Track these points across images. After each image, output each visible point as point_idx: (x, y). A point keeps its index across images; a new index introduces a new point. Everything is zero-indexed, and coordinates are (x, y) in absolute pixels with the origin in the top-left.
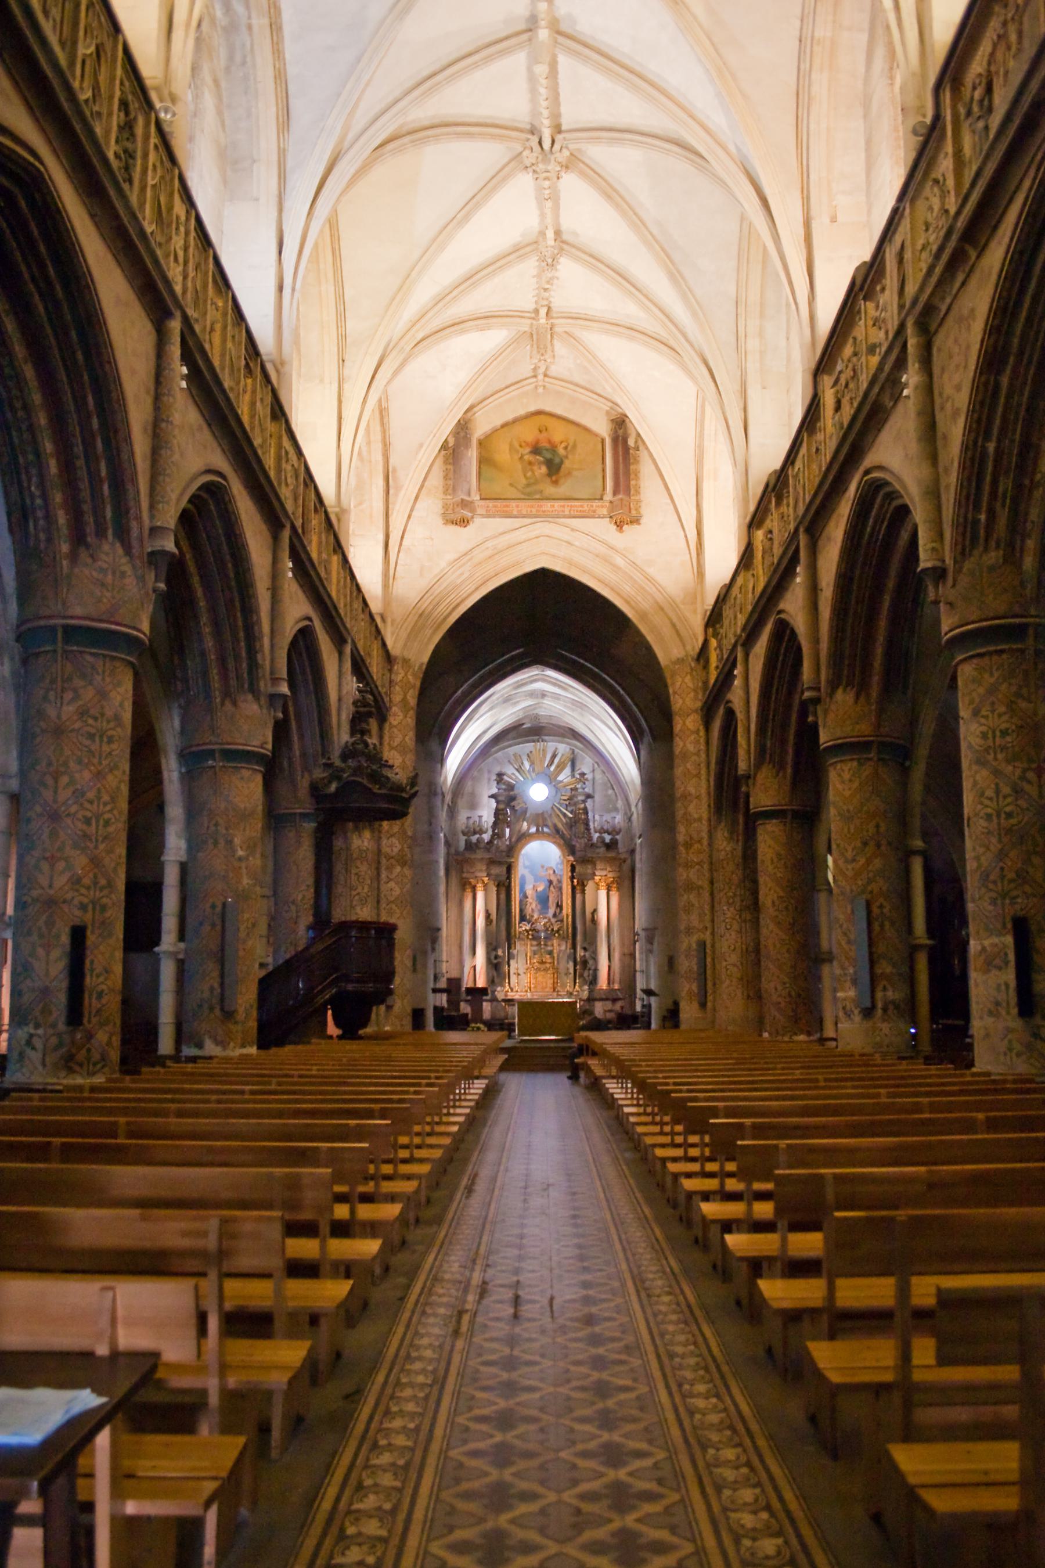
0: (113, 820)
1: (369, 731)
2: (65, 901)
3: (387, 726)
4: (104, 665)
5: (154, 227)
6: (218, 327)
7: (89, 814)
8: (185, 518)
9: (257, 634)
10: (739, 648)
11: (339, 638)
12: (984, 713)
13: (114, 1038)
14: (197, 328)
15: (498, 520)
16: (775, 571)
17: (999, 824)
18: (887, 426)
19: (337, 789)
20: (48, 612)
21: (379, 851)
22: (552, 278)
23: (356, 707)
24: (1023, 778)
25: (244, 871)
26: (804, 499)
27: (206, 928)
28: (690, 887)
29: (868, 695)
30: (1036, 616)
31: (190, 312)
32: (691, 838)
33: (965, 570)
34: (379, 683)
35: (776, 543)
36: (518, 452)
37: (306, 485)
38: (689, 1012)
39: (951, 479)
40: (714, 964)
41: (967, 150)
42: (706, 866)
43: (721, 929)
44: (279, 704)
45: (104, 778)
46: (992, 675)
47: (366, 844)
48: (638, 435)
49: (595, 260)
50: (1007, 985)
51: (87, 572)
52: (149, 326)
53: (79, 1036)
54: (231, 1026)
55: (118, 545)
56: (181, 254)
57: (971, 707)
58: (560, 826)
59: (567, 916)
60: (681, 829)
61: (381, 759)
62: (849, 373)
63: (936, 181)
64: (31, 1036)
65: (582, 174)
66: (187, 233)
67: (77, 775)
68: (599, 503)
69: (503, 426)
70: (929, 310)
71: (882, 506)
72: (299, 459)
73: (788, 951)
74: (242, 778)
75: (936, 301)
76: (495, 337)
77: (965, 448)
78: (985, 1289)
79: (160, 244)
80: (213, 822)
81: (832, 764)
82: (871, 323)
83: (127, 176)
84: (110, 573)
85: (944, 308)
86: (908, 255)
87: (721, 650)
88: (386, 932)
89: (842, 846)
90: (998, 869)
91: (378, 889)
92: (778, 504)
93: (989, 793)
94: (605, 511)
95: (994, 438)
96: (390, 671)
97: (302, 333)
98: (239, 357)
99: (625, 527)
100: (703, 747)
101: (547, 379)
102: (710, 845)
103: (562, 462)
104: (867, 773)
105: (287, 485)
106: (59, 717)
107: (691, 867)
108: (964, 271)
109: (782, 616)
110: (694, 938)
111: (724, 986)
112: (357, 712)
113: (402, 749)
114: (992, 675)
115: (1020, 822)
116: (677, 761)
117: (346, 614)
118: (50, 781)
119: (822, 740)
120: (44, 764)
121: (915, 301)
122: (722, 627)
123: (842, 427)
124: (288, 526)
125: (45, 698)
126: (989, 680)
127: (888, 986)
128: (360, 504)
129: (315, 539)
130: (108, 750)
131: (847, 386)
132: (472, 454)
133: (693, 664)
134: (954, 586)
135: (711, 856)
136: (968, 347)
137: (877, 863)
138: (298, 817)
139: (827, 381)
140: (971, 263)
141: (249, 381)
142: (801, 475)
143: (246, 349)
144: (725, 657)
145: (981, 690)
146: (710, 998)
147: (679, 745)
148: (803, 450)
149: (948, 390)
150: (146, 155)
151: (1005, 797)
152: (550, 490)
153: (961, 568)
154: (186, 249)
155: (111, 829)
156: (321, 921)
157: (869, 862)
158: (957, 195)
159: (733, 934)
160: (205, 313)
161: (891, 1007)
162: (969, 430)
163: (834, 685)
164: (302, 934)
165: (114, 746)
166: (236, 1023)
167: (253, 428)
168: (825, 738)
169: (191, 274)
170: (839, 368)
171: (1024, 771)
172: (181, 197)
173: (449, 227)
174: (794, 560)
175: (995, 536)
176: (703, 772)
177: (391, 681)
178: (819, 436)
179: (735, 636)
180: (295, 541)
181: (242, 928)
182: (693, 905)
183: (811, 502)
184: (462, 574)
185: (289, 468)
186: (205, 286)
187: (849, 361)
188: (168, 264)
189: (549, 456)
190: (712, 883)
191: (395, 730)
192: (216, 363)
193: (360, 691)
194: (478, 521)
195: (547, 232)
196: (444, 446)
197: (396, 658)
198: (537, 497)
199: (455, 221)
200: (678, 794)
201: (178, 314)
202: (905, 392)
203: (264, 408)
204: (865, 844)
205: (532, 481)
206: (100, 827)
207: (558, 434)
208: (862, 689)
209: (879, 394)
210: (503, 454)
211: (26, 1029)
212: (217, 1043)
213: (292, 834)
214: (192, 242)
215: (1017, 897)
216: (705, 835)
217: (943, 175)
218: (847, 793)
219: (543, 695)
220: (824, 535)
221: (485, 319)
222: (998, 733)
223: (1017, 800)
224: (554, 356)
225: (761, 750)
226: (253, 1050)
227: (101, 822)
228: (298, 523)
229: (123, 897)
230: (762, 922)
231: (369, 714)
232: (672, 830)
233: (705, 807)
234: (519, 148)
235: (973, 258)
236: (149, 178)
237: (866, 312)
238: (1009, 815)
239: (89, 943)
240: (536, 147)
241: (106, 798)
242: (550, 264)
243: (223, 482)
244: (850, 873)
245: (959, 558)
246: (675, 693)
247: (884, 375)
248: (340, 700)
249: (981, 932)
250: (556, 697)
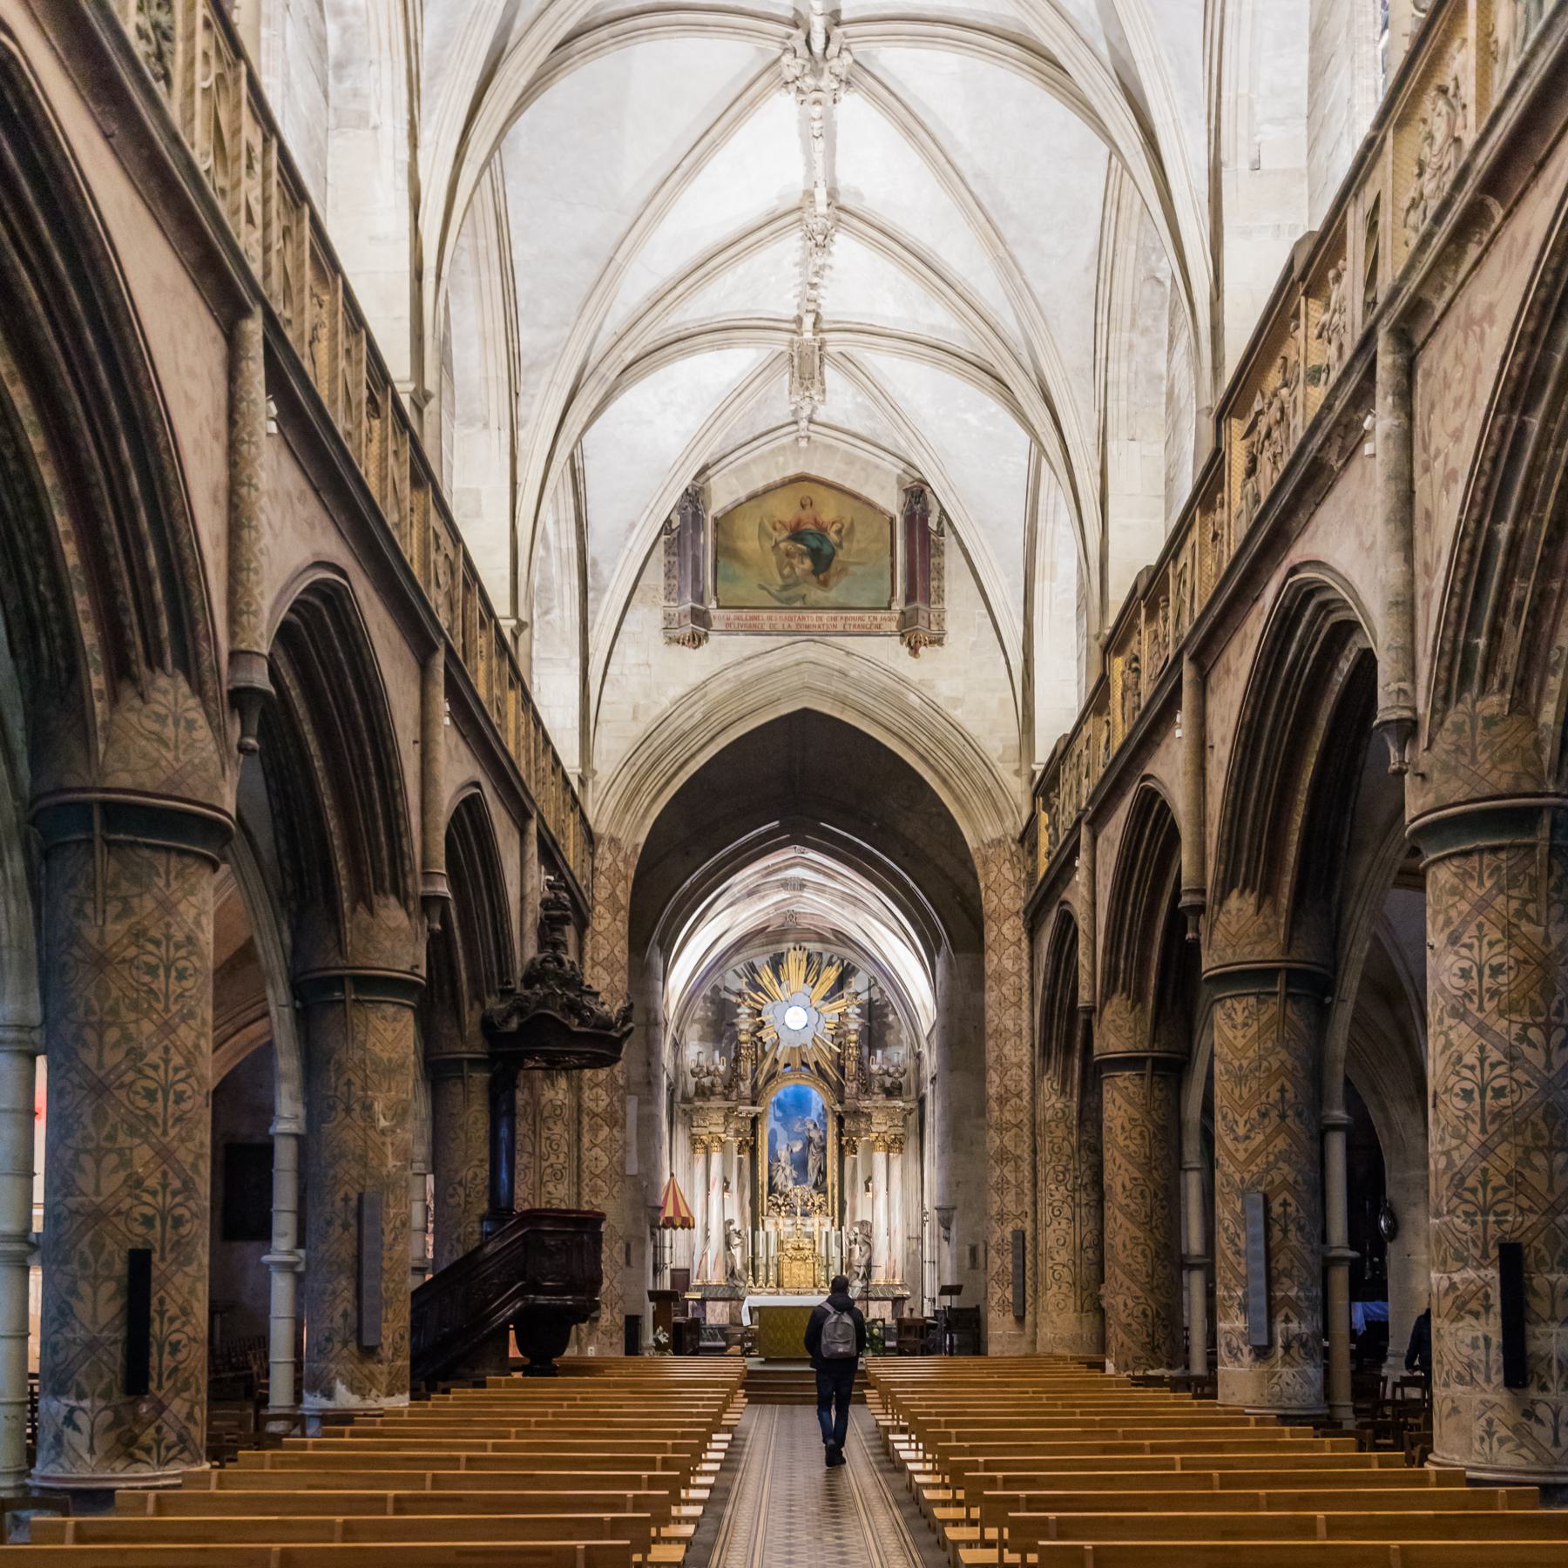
0: (189, 1093)
1: (565, 945)
2: (119, 1213)
3: (588, 932)
4: (168, 863)
5: (211, 161)
6: (324, 333)
8: (285, 634)
10: (1084, 829)
11: (521, 811)
12: (1465, 940)
13: (197, 1409)
14: (290, 335)
15: (742, 638)
16: (1142, 718)
17: (1483, 1105)
18: (1330, 500)
19: (521, 1026)
20: (76, 783)
21: (579, 1106)
22: (823, 267)
23: (546, 909)
24: (1522, 1038)
25: (389, 1150)
26: (1192, 610)
27: (337, 1230)
28: (1003, 1156)
29: (1275, 904)
30: (1557, 795)
31: (278, 307)
32: (1007, 1090)
33: (1447, 724)
34: (577, 873)
35: (1144, 676)
36: (770, 537)
37: (466, 586)
38: (999, 1327)
39: (1434, 586)
40: (1036, 1265)
41: (1502, 32)
42: (1026, 1131)
43: (1045, 1214)
44: (436, 912)
45: (174, 1031)
46: (1481, 884)
47: (561, 1096)
48: (943, 511)
49: (887, 238)
50: (1487, 1340)
51: (133, 718)
52: (213, 330)
53: (144, 1408)
54: (372, 1367)
55: (181, 678)
56: (257, 210)
57: (1447, 931)
58: (824, 1065)
59: (1519, 605)
60: (993, 1076)
61: (582, 983)
62: (1274, 413)
63: (1443, 91)
64: (72, 1410)
65: (870, 93)
66: (266, 175)
67: (132, 1028)
68: (884, 614)
69: (751, 498)
70: (1417, 308)
71: (1311, 623)
72: (455, 546)
73: (1143, 1253)
74: (384, 1018)
75: (1427, 294)
76: (738, 361)
77: (1461, 536)
79: (223, 192)
80: (343, 1080)
81: (1220, 1000)
82: (1316, 332)
83: (159, 69)
84: (170, 721)
85: (1440, 306)
86: (1385, 219)
87: (1056, 829)
88: (586, 1225)
89: (1230, 1116)
90: (1478, 1172)
91: (579, 1158)
92: (1151, 617)
93: (1470, 1059)
94: (893, 626)
95: (1510, 515)
96: (593, 855)
97: (455, 350)
98: (358, 384)
99: (922, 650)
100: (1025, 965)
101: (812, 427)
102: (1033, 1099)
103: (834, 553)
104: (1270, 1013)
105: (438, 585)
106: (101, 941)
107: (1007, 1130)
108: (1480, 242)
109: (1150, 784)
110: (1009, 1230)
111: (1050, 1293)
112: (547, 917)
113: (609, 965)
114: (1481, 884)
115: (1513, 1104)
116: (989, 983)
117: (529, 776)
118: (90, 1035)
120: (81, 1011)
121: (1395, 292)
122: (1058, 796)
123: (1257, 501)
124: (442, 649)
125: (79, 912)
126: (1476, 890)
127: (1291, 1314)
128: (546, 612)
129: (482, 666)
130: (179, 991)
131: (1268, 435)
132: (707, 538)
133: (1013, 848)
134: (1428, 748)
135: (1033, 1115)
136: (1478, 369)
137: (1281, 1143)
138: (465, 1064)
139: (1237, 427)
140: (1493, 227)
141: (376, 423)
142: (1188, 575)
143: (368, 371)
144: (1061, 840)
145: (1464, 907)
146: (1029, 1309)
147: (992, 962)
148: (1194, 535)
149: (1440, 439)
150: (190, 37)
151: (1493, 1066)
152: (816, 594)
153: (1442, 723)
154: (266, 201)
155: (186, 1106)
156: (500, 1210)
157: (1268, 1141)
158: (1479, 114)
159: (1064, 1222)
160: (302, 311)
161: (1295, 1344)
162: (1468, 505)
163: (1226, 885)
164: (472, 1230)
165: (188, 984)
166: (380, 1362)
167: (384, 498)
168: (1209, 962)
169: (277, 245)
170: (1257, 407)
171: (1525, 1027)
172: (253, 111)
173: (669, 185)
174: (1172, 704)
175: (1499, 672)
176: (1026, 997)
177: (594, 870)
178: (1220, 516)
179: (1078, 810)
180: (453, 670)
181: (387, 1228)
182: (1008, 1182)
183: (1203, 616)
184: (691, 716)
185: (441, 559)
186: (300, 266)
187: (1275, 395)
188: (237, 225)
189: (815, 543)
190: (1035, 1152)
191: (601, 939)
192: (323, 392)
193: (551, 887)
194: (714, 638)
195: (817, 191)
196: (667, 527)
197: (601, 837)
198: (798, 604)
199: (679, 172)
200: (990, 1029)
201: (258, 311)
202: (1368, 448)
203: (400, 466)
204: (1264, 1115)
205: (790, 581)
206: (170, 1103)
207: (829, 511)
208: (1267, 891)
209: (1320, 449)
210: (750, 542)
211: (64, 1401)
212: (353, 1389)
213: (459, 1089)
214: (274, 190)
215: (1506, 1213)
216: (1026, 1084)
217: (1456, 79)
218: (1240, 1043)
219: (801, 885)
220: (1220, 666)
221: (723, 332)
222: (1487, 971)
223: (1511, 1069)
224: (824, 391)
225: (1111, 974)
226: (402, 1401)
227: (172, 1097)
228: (457, 645)
229: (207, 1204)
230: (1108, 1213)
231: (565, 920)
232: (981, 1075)
233: (1026, 1048)
234: (776, 50)
235: (1498, 219)
236: (198, 76)
237: (1307, 314)
238: (1499, 1093)
239: (155, 1273)
240: (802, 50)
241: (177, 1060)
242: (821, 243)
243: (344, 582)
244: (1241, 1156)
245: (1439, 705)
246: (987, 888)
247: (1333, 416)
248: (523, 898)
249: (1449, 1261)
250: (820, 888)
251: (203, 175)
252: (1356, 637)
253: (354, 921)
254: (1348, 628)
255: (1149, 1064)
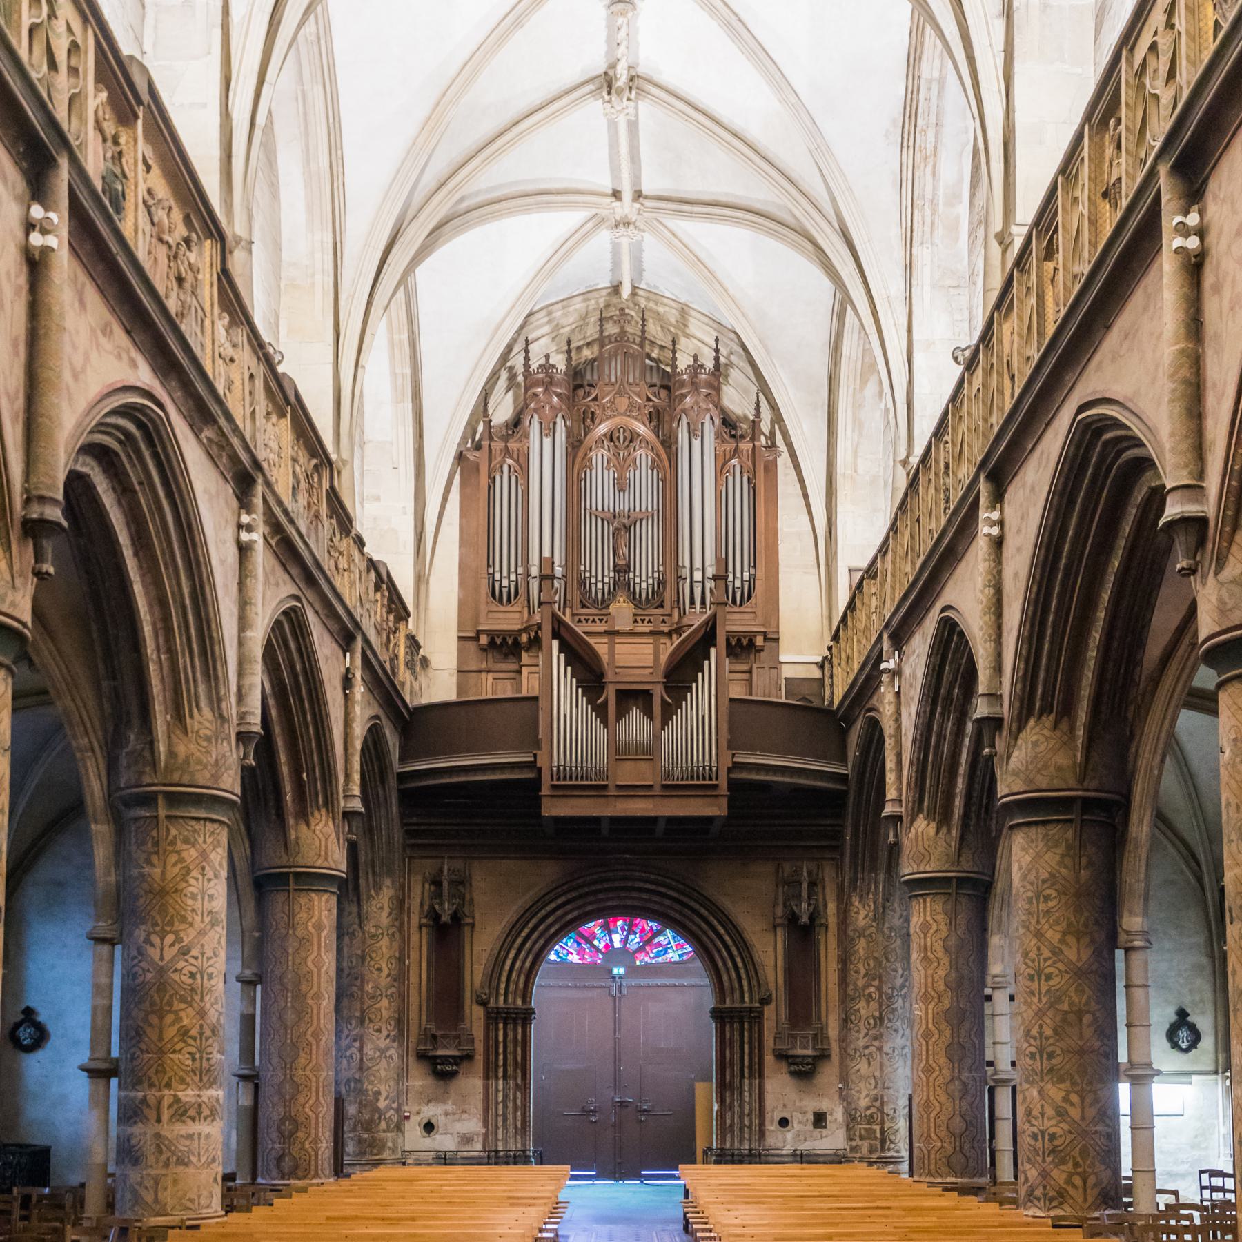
7: (194, 970)
9: (151, 587)
78: (285, 741)
119: (1002, 789)
151: (1045, 960)
208: (944, 819)
251: (36, 82)
252: (1149, 474)
253: (298, 832)
254: (1145, 464)
255: (954, 881)
